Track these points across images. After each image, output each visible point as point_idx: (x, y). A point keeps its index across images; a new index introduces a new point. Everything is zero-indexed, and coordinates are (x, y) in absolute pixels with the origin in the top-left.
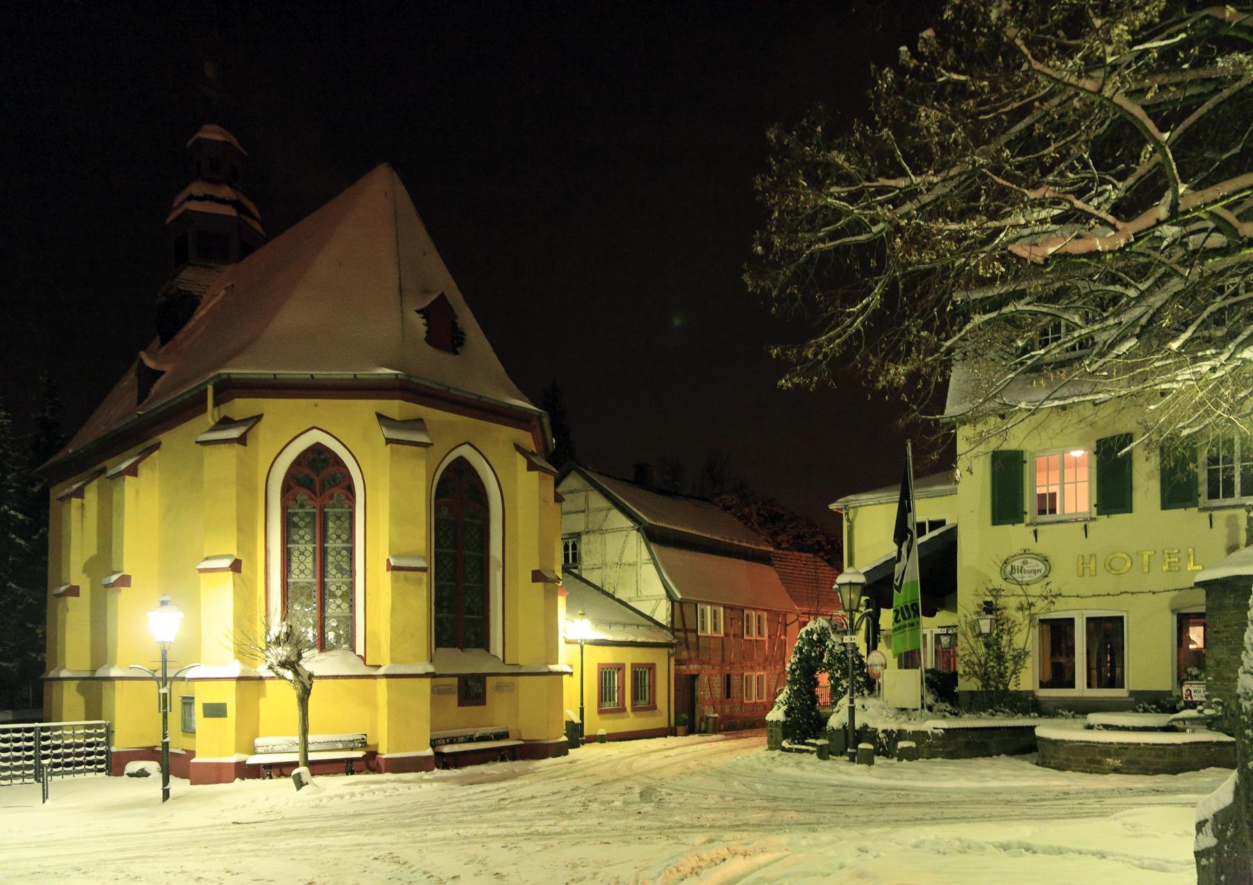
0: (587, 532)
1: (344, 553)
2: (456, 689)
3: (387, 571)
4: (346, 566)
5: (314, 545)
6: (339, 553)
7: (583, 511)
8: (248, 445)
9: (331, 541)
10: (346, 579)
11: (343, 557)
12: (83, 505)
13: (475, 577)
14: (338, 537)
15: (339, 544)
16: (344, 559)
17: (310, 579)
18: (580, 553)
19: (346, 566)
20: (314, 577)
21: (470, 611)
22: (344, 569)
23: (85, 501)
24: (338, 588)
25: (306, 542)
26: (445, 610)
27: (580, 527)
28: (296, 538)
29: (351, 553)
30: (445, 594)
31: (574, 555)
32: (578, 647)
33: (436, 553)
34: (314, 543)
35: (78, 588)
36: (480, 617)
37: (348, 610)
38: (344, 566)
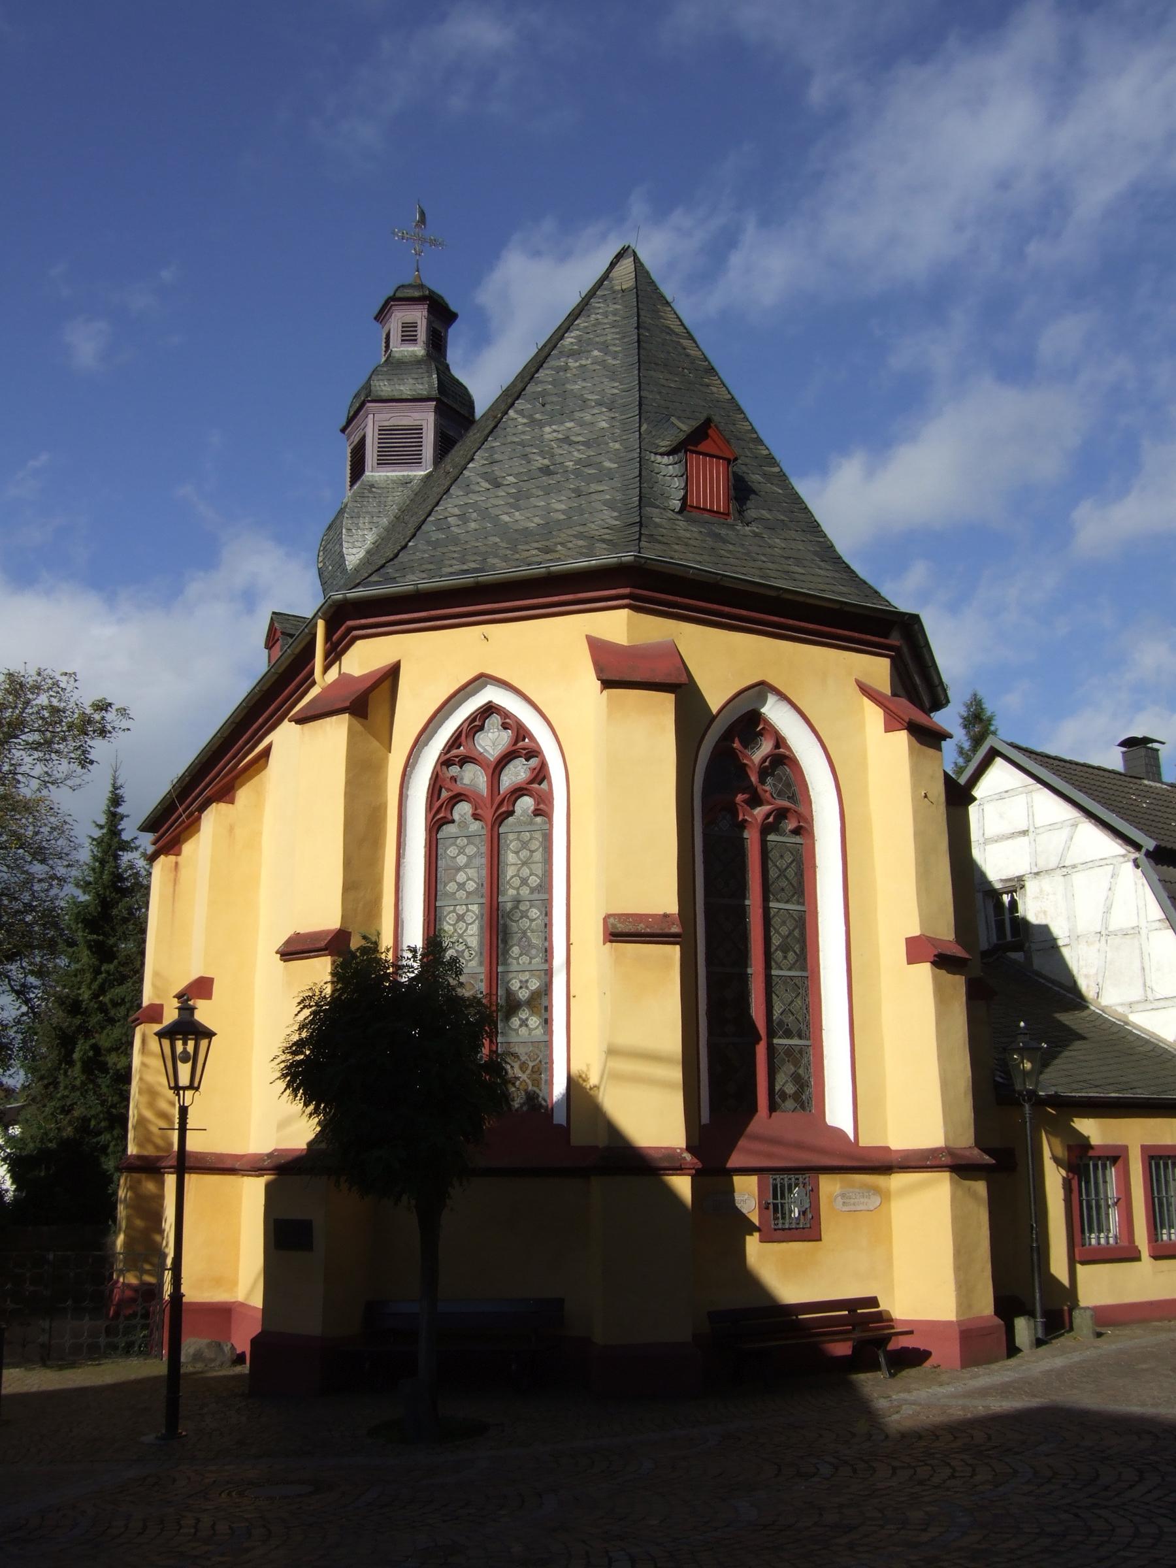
7: (1025, 833)
12: (177, 863)
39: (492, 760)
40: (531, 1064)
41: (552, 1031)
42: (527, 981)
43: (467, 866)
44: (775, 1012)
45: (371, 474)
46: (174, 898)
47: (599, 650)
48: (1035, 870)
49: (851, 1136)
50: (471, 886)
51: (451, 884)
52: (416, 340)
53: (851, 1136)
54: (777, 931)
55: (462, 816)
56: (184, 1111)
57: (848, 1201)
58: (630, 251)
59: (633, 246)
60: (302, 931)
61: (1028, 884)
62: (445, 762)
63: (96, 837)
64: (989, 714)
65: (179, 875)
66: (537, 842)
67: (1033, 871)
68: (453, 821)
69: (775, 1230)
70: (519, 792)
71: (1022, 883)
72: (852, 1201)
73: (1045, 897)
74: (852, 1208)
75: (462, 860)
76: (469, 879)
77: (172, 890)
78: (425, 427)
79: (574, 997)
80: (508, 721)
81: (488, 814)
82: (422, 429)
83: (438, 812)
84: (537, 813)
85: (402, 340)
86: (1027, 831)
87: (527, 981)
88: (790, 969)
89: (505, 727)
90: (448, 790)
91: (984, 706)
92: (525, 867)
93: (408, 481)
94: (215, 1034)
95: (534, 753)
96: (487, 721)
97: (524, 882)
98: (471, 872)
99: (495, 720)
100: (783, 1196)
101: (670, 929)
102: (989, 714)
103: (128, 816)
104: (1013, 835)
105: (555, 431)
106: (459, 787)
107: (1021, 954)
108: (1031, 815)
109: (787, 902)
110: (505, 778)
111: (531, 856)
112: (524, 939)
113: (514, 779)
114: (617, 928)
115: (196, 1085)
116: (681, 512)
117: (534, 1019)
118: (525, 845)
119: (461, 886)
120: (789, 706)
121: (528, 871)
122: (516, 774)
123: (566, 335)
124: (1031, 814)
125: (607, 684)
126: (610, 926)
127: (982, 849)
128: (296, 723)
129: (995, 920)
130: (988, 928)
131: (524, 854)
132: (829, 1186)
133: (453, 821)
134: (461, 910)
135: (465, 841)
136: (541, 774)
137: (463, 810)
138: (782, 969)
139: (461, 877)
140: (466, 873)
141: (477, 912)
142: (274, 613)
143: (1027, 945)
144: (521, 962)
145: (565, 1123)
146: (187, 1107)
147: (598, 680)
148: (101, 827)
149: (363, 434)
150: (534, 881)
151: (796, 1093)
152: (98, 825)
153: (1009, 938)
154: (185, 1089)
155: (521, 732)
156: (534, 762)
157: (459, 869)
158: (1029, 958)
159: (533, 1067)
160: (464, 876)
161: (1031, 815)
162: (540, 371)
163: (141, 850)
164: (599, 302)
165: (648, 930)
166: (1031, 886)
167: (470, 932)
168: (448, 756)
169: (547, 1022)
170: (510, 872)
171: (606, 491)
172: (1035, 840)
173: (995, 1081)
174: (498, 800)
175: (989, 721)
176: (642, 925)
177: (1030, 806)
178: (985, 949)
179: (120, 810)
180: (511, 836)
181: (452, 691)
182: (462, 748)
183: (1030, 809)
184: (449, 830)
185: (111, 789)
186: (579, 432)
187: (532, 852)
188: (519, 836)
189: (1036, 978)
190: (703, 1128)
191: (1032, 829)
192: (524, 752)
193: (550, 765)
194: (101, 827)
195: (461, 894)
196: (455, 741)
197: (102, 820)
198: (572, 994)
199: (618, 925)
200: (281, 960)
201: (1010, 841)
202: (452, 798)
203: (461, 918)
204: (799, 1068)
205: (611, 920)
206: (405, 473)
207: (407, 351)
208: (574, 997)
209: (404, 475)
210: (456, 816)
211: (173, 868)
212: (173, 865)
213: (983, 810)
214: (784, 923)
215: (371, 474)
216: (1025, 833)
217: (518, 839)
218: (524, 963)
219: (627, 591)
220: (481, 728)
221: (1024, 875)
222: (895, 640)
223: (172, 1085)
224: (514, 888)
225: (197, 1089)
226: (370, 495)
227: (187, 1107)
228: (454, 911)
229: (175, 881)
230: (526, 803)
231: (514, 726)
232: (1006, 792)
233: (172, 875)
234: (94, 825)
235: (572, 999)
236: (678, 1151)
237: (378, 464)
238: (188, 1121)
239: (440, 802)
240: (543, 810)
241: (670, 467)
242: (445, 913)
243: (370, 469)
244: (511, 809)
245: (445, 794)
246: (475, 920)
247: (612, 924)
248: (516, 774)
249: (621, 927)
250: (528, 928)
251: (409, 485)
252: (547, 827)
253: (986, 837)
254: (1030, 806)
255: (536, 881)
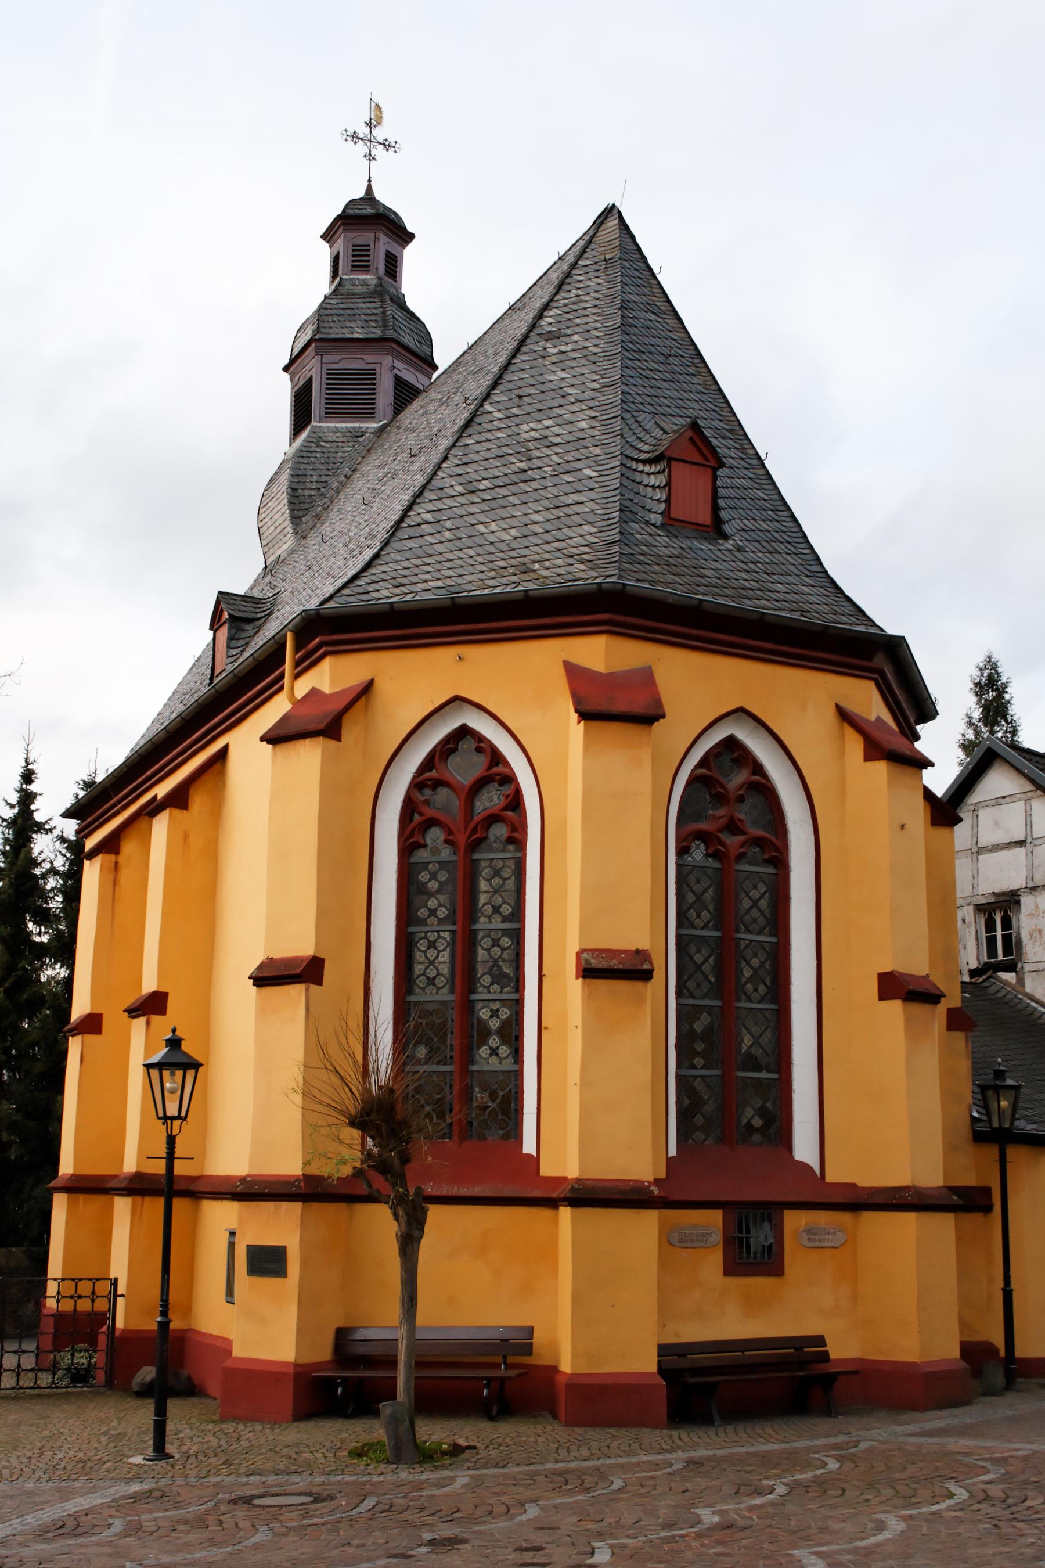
0: (1034, 889)
1: (506, 942)
2: (717, 1237)
3: (577, 978)
4: (507, 970)
5: (453, 928)
6: (496, 943)
7: (1021, 843)
8: (343, 738)
9: (482, 919)
10: (509, 995)
11: (503, 949)
12: (116, 863)
13: (762, 989)
14: (496, 910)
15: (497, 923)
16: (506, 955)
17: (444, 995)
18: (1019, 934)
19: (507, 970)
20: (452, 991)
21: (751, 1063)
22: (506, 975)
23: (121, 858)
24: (494, 1014)
25: (441, 921)
26: (699, 1061)
27: (1014, 880)
28: (423, 913)
29: (518, 943)
30: (698, 1027)
31: (1007, 939)
32: (73, 1283)
33: (678, 937)
34: (454, 924)
35: (883, 995)
36: (775, 1076)
37: (511, 1059)
38: (505, 970)
39: (465, 783)
40: (501, 1093)
41: (523, 1062)
42: (498, 1010)
43: (439, 891)
44: (743, 1045)
45: (319, 424)
46: (114, 899)
47: (574, 673)
48: (1031, 885)
49: (817, 1170)
50: (442, 912)
51: (422, 910)
52: (368, 266)
53: (817, 1171)
54: (748, 963)
55: (435, 841)
56: (171, 1140)
57: (813, 1237)
58: (615, 211)
59: (617, 204)
60: (276, 956)
61: (1023, 899)
62: (418, 784)
63: (6, 817)
64: (1004, 680)
65: (118, 876)
66: (509, 870)
67: (1028, 886)
68: (425, 846)
69: (739, 1264)
70: (493, 819)
71: (1016, 898)
72: (817, 1237)
73: (1041, 915)
74: (817, 1244)
75: (433, 885)
76: (440, 905)
77: (111, 892)
78: (378, 371)
79: (546, 1028)
80: (482, 744)
81: (462, 839)
82: (374, 374)
83: (408, 838)
84: (511, 840)
85: (353, 266)
86: (1025, 841)
87: (498, 1010)
88: (759, 1002)
89: (479, 750)
90: (421, 814)
91: (1000, 670)
92: (497, 895)
93: (359, 434)
94: (201, 1065)
95: (509, 779)
96: (460, 744)
97: (496, 910)
98: (442, 898)
99: (467, 745)
100: (748, 1231)
101: (642, 965)
102: (1004, 680)
103: (41, 794)
104: (1009, 845)
105: (533, 430)
106: (430, 812)
107: (1014, 974)
108: (1029, 824)
109: (759, 934)
110: (478, 803)
111: (504, 884)
112: (495, 968)
113: (487, 804)
114: (591, 964)
115: (183, 1114)
116: (663, 526)
117: (505, 1048)
118: (497, 873)
119: (433, 912)
120: (766, 733)
121: (500, 899)
122: (491, 800)
123: (545, 314)
124: (1029, 823)
125: (585, 715)
126: (583, 962)
127: (975, 858)
128: (268, 743)
129: (987, 937)
130: (978, 945)
131: (496, 881)
132: (794, 1221)
133: (425, 846)
134: (432, 937)
135: (437, 866)
136: (516, 802)
137: (435, 836)
138: (751, 1001)
139: (432, 903)
140: (438, 900)
141: (448, 939)
142: (220, 593)
143: (1019, 965)
144: (492, 991)
145: (534, 1153)
146: (175, 1136)
147: (576, 712)
148: (12, 806)
149: (308, 376)
150: (506, 910)
151: (762, 1127)
152: (8, 804)
153: (1000, 957)
154: (173, 1118)
155: (496, 757)
156: (508, 790)
157: (431, 895)
158: (1021, 981)
159: (503, 1096)
160: (436, 902)
161: (1029, 824)
162: (518, 356)
163: (56, 832)
164: (580, 275)
165: (621, 966)
166: (1027, 902)
167: (441, 959)
168: (420, 778)
169: (518, 1053)
170: (483, 899)
171: (590, 504)
172: (1032, 852)
173: (972, 1116)
174: (472, 825)
175: (1005, 686)
176: (615, 961)
177: (1028, 815)
178: (972, 968)
179: (33, 788)
180: (483, 864)
181: (426, 713)
182: (434, 771)
183: (1028, 817)
184: (422, 855)
185: (24, 764)
186: (557, 433)
187: (505, 880)
188: (491, 863)
189: (1028, 1001)
190: (669, 1160)
191: (1029, 840)
192: (498, 778)
193: (524, 793)
194: (12, 806)
195: (433, 920)
196: (428, 764)
197: (14, 798)
198: (544, 1025)
199: (593, 961)
200: (254, 985)
201: (1005, 852)
202: (425, 821)
203: (432, 945)
204: (767, 1101)
205: (585, 955)
206: (357, 425)
207: (358, 279)
208: (546, 1028)
209: (354, 428)
210: (428, 841)
211: (113, 870)
212: (113, 865)
213: (977, 816)
214: (755, 955)
215: (319, 424)
216: (1021, 843)
217: (490, 866)
218: (495, 992)
219: (606, 616)
220: (454, 750)
221: (1019, 889)
222: (880, 660)
223: (161, 1114)
224: (485, 916)
225: (185, 1119)
226: (318, 450)
227: (175, 1136)
228: (425, 937)
229: (115, 883)
230: (499, 831)
231: (489, 750)
232: (1004, 797)
233: (111, 876)
234: (5, 803)
235: (544, 1033)
236: (646, 1184)
237: (326, 413)
238: (176, 1150)
239: (412, 826)
240: (517, 840)
241: (652, 477)
242: (416, 940)
243: (318, 419)
244: (484, 835)
245: (417, 818)
246: (446, 948)
247: (586, 960)
248: (491, 800)
249: (594, 963)
250: (500, 957)
251: (361, 439)
252: (519, 855)
253: (980, 845)
254: (1028, 815)
255: (508, 910)
